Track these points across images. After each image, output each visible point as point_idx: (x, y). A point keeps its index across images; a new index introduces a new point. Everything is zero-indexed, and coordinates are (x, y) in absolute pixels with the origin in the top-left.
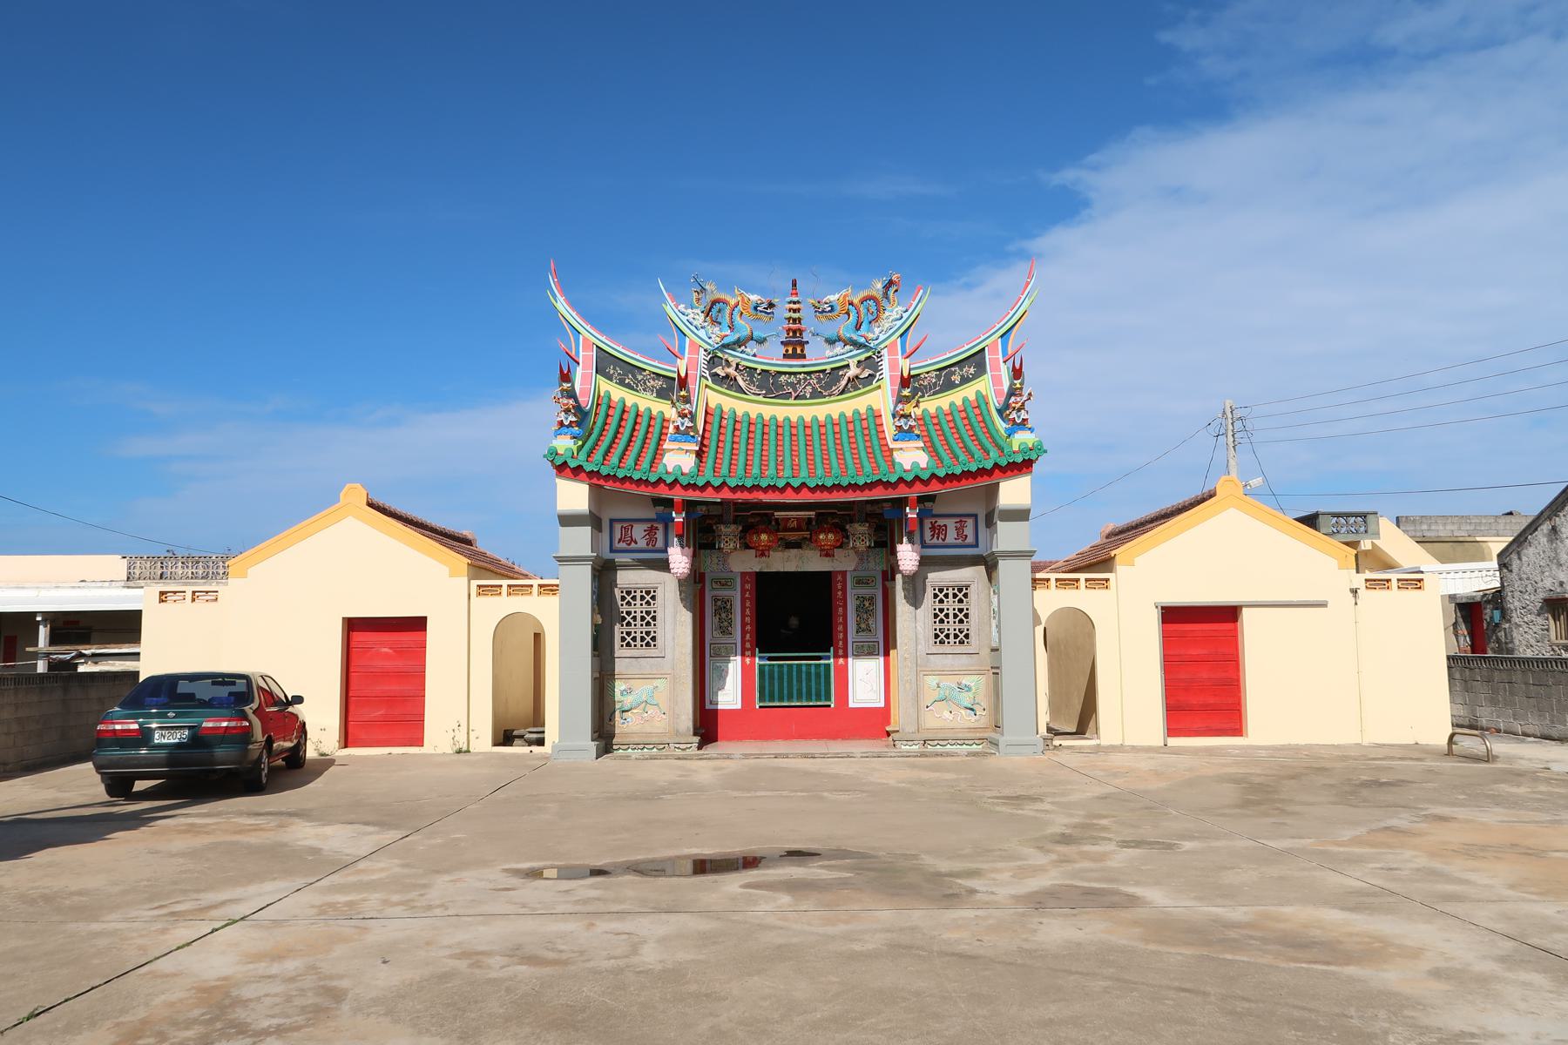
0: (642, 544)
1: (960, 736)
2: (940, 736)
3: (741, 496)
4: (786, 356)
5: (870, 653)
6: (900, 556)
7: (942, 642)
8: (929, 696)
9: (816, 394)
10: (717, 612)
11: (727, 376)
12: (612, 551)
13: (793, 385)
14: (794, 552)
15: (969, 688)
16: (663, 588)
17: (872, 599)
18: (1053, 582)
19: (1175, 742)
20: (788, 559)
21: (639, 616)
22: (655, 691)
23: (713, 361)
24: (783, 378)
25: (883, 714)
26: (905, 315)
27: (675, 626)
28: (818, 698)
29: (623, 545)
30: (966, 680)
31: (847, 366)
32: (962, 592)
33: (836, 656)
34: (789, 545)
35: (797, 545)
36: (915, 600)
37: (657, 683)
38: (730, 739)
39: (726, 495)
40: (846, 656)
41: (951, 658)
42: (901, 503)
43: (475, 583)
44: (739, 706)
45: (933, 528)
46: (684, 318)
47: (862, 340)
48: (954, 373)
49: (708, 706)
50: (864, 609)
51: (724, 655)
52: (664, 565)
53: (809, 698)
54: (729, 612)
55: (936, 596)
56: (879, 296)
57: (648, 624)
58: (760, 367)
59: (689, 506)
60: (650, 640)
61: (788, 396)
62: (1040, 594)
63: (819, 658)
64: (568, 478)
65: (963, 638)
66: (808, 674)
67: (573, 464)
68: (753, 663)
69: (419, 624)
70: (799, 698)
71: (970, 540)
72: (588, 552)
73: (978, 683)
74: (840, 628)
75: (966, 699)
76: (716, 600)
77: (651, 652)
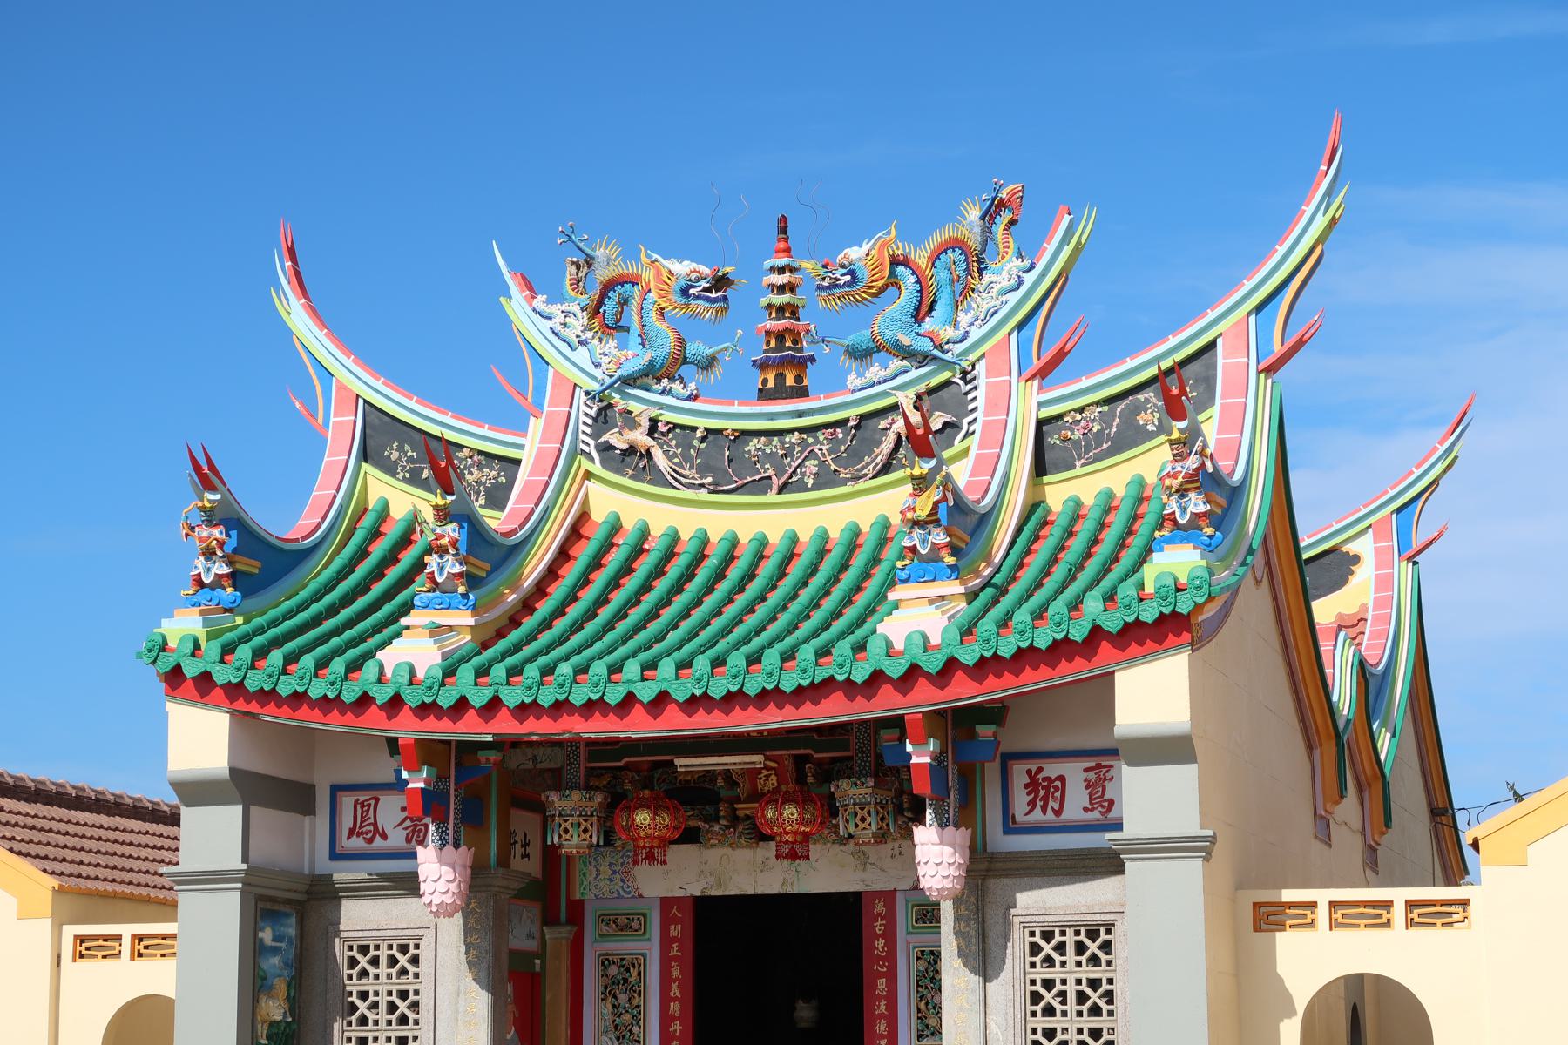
3: (535, 728)
4: (764, 395)
6: (921, 853)
9: (826, 479)
10: (607, 992)
11: (632, 450)
12: (335, 856)
13: (777, 463)
20: (764, 866)
21: (383, 1000)
23: (604, 417)
24: (754, 445)
26: (1029, 279)
29: (357, 843)
31: (895, 408)
36: (984, 964)
39: (505, 725)
43: (70, 931)
45: (1033, 785)
46: (545, 325)
47: (925, 345)
48: (1139, 408)
52: (409, 884)
54: (635, 990)
56: (974, 240)
57: (403, 1020)
58: (702, 423)
59: (430, 752)
61: (761, 486)
62: (1287, 942)
64: (188, 700)
67: (191, 669)
72: (236, 863)
76: (605, 962)
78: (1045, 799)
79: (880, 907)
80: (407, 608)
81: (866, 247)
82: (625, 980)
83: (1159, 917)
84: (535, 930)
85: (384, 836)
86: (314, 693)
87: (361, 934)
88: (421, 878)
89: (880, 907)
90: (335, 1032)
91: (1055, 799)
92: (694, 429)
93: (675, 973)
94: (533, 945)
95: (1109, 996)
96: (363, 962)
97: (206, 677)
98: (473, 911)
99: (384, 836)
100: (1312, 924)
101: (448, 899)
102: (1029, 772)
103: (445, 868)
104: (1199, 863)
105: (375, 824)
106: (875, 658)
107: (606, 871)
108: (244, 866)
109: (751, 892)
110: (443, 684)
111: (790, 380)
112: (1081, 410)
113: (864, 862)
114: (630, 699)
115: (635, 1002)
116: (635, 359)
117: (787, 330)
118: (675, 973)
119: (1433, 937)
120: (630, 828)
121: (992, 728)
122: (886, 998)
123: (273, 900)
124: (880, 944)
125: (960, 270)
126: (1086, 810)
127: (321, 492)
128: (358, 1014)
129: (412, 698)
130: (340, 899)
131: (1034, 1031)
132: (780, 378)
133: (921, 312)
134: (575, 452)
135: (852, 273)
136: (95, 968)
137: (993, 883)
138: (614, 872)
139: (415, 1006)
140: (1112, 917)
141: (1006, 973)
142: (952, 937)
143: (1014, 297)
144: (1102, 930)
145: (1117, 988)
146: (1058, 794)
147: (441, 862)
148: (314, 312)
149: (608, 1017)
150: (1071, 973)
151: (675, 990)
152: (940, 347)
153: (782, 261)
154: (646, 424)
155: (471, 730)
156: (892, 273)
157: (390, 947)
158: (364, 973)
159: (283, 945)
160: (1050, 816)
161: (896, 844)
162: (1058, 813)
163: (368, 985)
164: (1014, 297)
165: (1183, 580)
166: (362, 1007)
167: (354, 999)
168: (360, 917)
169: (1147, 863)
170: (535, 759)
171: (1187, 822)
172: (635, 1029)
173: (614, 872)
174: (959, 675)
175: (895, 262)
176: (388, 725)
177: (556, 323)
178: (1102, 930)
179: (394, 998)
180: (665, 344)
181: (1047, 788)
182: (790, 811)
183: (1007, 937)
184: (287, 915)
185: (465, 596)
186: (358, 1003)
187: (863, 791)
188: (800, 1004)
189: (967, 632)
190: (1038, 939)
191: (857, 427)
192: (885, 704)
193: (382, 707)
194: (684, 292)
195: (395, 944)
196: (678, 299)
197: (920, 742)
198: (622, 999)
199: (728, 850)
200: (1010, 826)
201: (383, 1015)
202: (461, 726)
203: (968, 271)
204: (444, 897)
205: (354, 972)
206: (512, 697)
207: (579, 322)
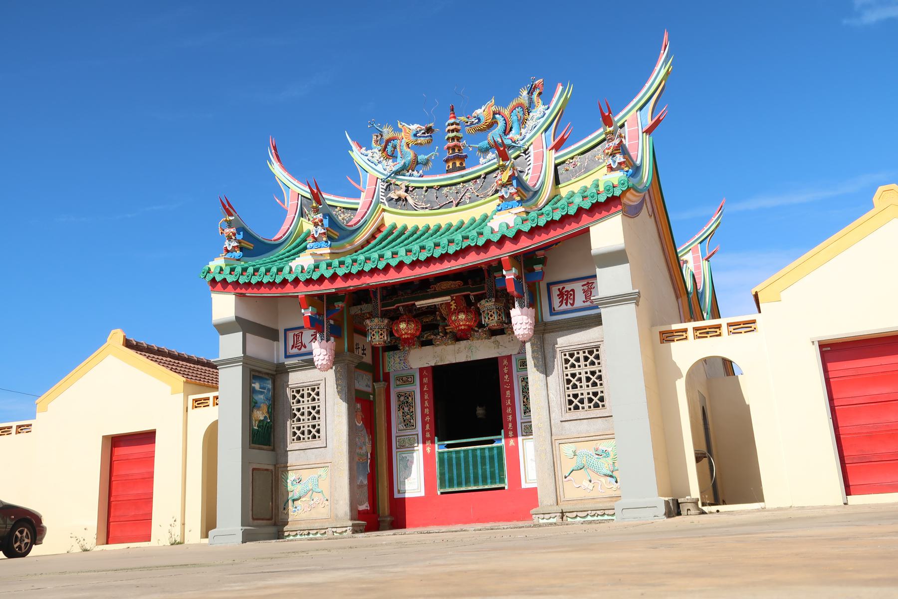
1: (601, 506)
2: (580, 507)
3: (353, 284)
7: (577, 408)
8: (566, 466)
10: (400, 407)
11: (399, 199)
12: (287, 357)
15: (606, 453)
18: (690, 333)
19: (854, 500)
20: (459, 351)
22: (321, 477)
26: (548, 112)
27: (335, 415)
29: (295, 351)
30: (603, 446)
33: (507, 437)
37: (321, 471)
39: (340, 284)
40: (515, 436)
41: (586, 423)
42: (497, 266)
44: (422, 494)
45: (561, 295)
46: (365, 158)
49: (396, 496)
51: (408, 447)
57: (314, 418)
59: (312, 300)
60: (315, 433)
63: (492, 442)
64: (219, 292)
66: (475, 456)
67: (218, 279)
68: (433, 450)
69: (148, 437)
70: (476, 482)
74: (509, 410)
75: (605, 465)
76: (399, 396)
78: (567, 300)
79: (505, 362)
80: (305, 248)
81: (483, 108)
83: (619, 335)
84: (370, 383)
85: (305, 347)
86: (265, 281)
92: (422, 188)
93: (426, 397)
94: (370, 390)
95: (600, 378)
96: (298, 396)
97: (225, 280)
99: (305, 347)
100: (686, 338)
101: (325, 362)
104: (633, 305)
106: (487, 235)
107: (398, 360)
110: (314, 271)
111: (458, 164)
112: (572, 158)
113: (497, 344)
114: (388, 266)
116: (400, 162)
117: (455, 146)
119: (744, 338)
120: (398, 330)
121: (541, 266)
123: (260, 372)
125: (521, 114)
127: (284, 227)
129: (302, 278)
130: (288, 372)
131: (569, 396)
132: (454, 164)
133: (507, 131)
134: (378, 203)
135: (479, 120)
136: (201, 410)
137: (547, 336)
141: (555, 372)
143: (542, 120)
145: (605, 395)
148: (285, 168)
150: (583, 370)
151: (427, 404)
152: (514, 142)
153: (452, 121)
154: (404, 188)
155: (327, 288)
156: (494, 118)
160: (569, 306)
162: (572, 305)
163: (300, 406)
164: (542, 120)
165: (616, 183)
166: (298, 414)
167: (295, 411)
168: (296, 379)
171: (626, 287)
174: (523, 238)
175: (494, 113)
177: (369, 157)
179: (310, 410)
180: (410, 155)
181: (567, 295)
182: (462, 316)
183: (554, 357)
185: (326, 242)
188: (478, 408)
189: (524, 221)
190: (568, 357)
191: (485, 178)
192: (493, 254)
193: (291, 283)
194: (415, 135)
196: (413, 138)
197: (508, 270)
198: (406, 409)
200: (552, 312)
202: (322, 287)
203: (524, 114)
206: (341, 272)
207: (378, 155)
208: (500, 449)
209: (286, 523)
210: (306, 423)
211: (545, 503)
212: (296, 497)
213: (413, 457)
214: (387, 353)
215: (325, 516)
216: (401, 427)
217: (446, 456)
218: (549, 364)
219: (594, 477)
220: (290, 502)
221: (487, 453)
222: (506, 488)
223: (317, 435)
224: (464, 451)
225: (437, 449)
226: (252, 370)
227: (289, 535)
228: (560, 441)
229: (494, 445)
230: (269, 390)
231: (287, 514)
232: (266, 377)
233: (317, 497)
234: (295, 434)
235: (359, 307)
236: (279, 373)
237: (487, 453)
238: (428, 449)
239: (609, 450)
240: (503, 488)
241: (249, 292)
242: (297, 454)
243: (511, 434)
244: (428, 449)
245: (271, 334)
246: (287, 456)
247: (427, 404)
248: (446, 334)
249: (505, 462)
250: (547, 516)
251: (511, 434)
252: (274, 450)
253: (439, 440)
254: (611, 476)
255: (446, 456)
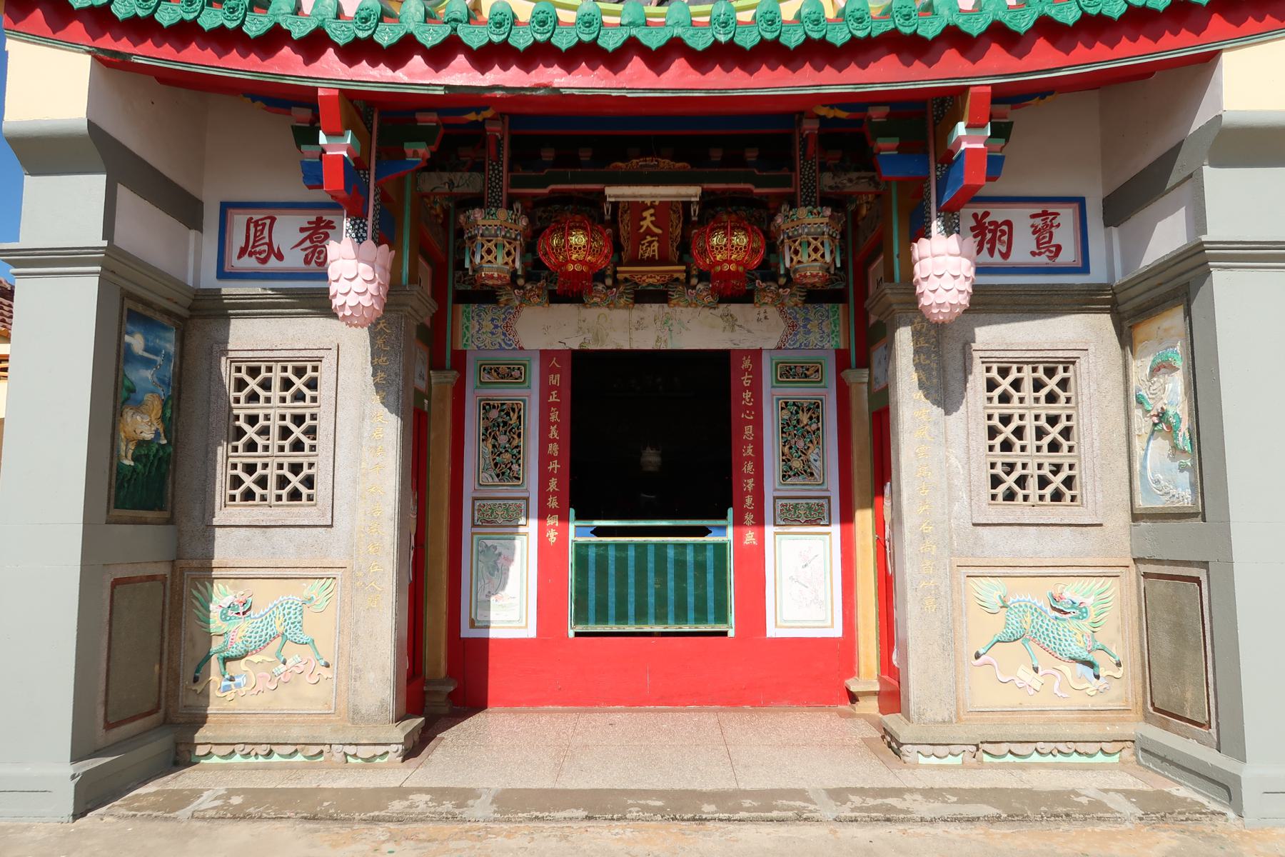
0: (294, 260)
2: (1016, 731)
5: (814, 517)
10: (489, 433)
12: (222, 274)
14: (652, 309)
15: (1079, 610)
16: (325, 347)
17: (815, 409)
20: (640, 325)
22: (304, 600)
25: (840, 653)
27: (363, 447)
28: (701, 617)
29: (249, 263)
30: (1072, 590)
32: (1054, 374)
33: (739, 522)
34: (643, 296)
35: (659, 296)
37: (312, 589)
38: (510, 703)
39: (460, 74)
40: (760, 522)
41: (1034, 536)
42: (947, 104)
44: (531, 632)
49: (466, 632)
50: (799, 425)
51: (502, 522)
53: (681, 617)
54: (515, 432)
55: (992, 385)
57: (298, 446)
59: (362, 108)
60: (298, 486)
63: (704, 531)
65: (1062, 489)
66: (680, 564)
68: (563, 537)
70: (661, 618)
71: (1069, 255)
73: (1107, 606)
74: (749, 468)
75: (1076, 637)
76: (487, 407)
77: (299, 512)
78: (992, 242)
79: (747, 363)
82: (505, 423)
84: (425, 372)
85: (280, 257)
87: (250, 354)
88: (332, 293)
89: (747, 363)
90: (219, 458)
91: (1002, 242)
93: (554, 417)
98: (381, 332)
99: (280, 257)
101: (366, 301)
102: (975, 216)
103: (362, 266)
105: (270, 244)
108: (105, 243)
109: (627, 347)
113: (731, 322)
115: (515, 443)
118: (554, 417)
122: (752, 442)
124: (747, 395)
126: (1033, 254)
128: (245, 439)
130: (228, 318)
138: (496, 327)
139: (311, 432)
140: (1075, 354)
142: (912, 368)
144: (1061, 367)
146: (1005, 238)
147: (359, 258)
149: (489, 456)
151: (554, 432)
157: (285, 369)
158: (253, 397)
159: (159, 359)
160: (997, 258)
161: (762, 310)
162: (1005, 256)
163: (258, 409)
166: (251, 432)
167: (241, 423)
168: (248, 336)
169: (1236, 273)
170: (451, 184)
172: (515, 467)
173: (496, 327)
176: (305, 71)
178: (1061, 367)
181: (994, 232)
183: (966, 371)
184: (165, 328)
186: (246, 427)
187: (819, 220)
195: (290, 366)
198: (503, 439)
199: (605, 311)
201: (274, 440)
202: (401, 75)
204: (361, 299)
205: (242, 395)
208: (720, 549)
209: (200, 720)
210: (273, 458)
211: (929, 715)
212: (233, 652)
213: (513, 549)
214: (462, 307)
215: (319, 708)
216: (486, 477)
217: (592, 553)
218: (955, 386)
219: (1043, 659)
220: (215, 664)
221: (690, 556)
222: (731, 633)
223: (304, 491)
224: (637, 545)
225: (572, 536)
226: (126, 295)
227: (209, 755)
228: (971, 571)
229: (708, 539)
230: (167, 357)
231: (205, 694)
232: (165, 320)
233: (295, 656)
234: (236, 482)
235: (446, 176)
236: (201, 316)
237: (690, 556)
238: (552, 536)
239: (1089, 601)
240: (725, 634)
241: (145, 53)
242: (241, 536)
243: (749, 518)
244: (552, 536)
245: (186, 210)
246: (211, 540)
247: (554, 432)
248: (616, 283)
249: (731, 577)
250: (941, 750)
251: (749, 518)
252: (170, 521)
253: (578, 517)
254: (1091, 664)
255: (592, 553)
